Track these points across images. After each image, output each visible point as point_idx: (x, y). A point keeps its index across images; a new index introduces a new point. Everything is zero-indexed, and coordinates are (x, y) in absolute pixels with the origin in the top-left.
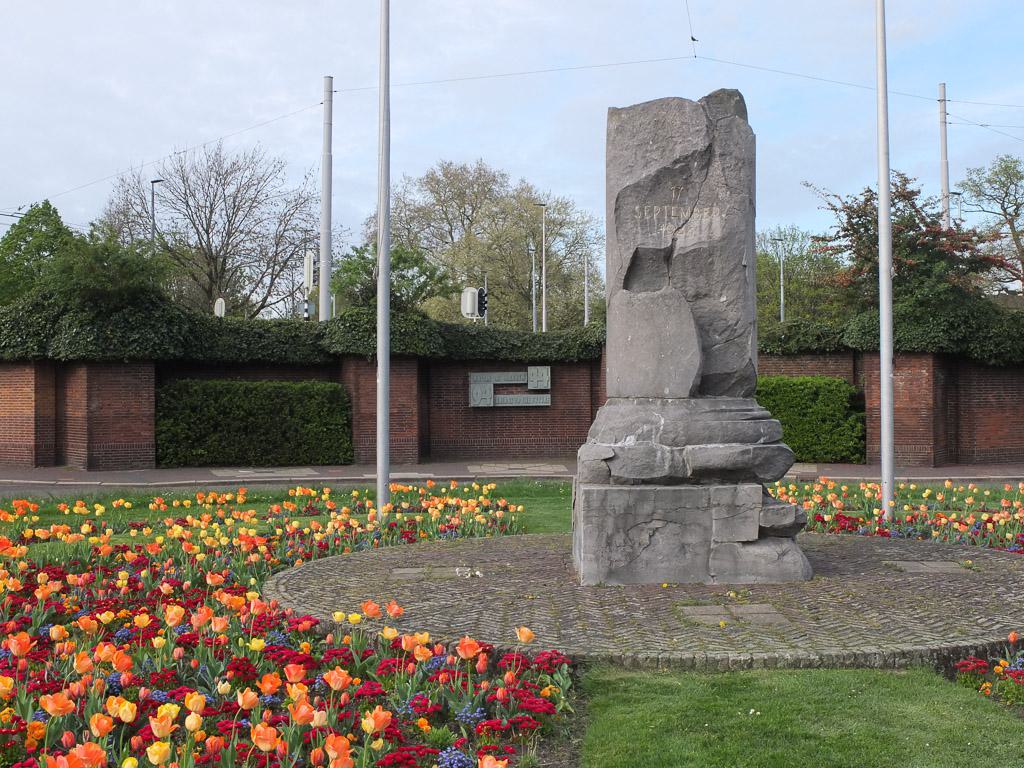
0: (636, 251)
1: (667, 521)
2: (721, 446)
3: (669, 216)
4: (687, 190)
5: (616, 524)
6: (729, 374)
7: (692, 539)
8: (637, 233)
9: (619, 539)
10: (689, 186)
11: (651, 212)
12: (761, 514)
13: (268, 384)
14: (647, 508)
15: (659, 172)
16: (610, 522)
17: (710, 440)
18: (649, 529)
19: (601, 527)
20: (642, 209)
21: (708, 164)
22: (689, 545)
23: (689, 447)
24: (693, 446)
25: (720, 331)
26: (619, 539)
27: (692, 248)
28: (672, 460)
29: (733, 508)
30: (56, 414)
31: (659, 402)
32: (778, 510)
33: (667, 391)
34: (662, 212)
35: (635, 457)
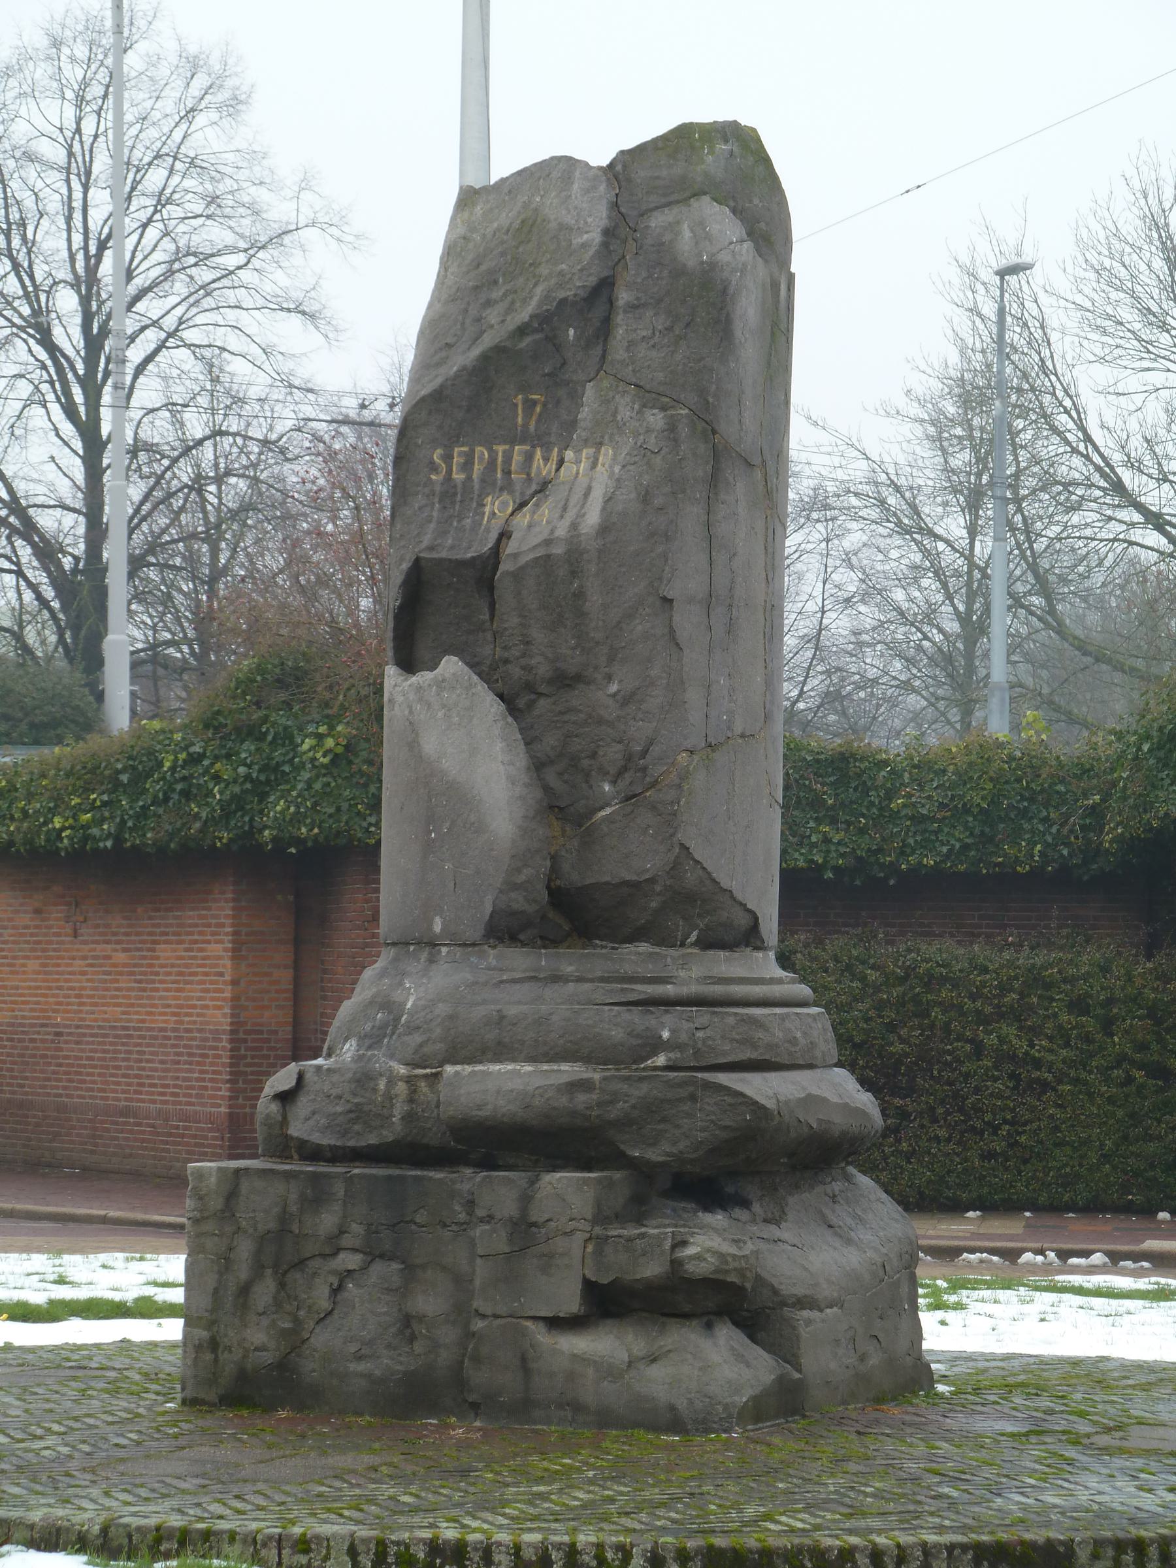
0: (417, 565)
1: (372, 1253)
2: (528, 1068)
3: (507, 473)
4: (558, 402)
5: (258, 1253)
6: (636, 885)
7: (429, 1302)
8: (429, 520)
9: (264, 1292)
10: (562, 392)
11: (467, 465)
12: (590, 1249)
13: (778, 1010)
14: (327, 1221)
15: (485, 358)
16: (245, 1249)
17: (501, 1051)
18: (334, 1272)
19: (225, 1262)
20: (448, 458)
21: (605, 329)
22: (421, 1318)
23: (449, 1069)
24: (458, 1068)
25: (613, 771)
26: (264, 1292)
27: (531, 556)
28: (411, 1100)
29: (524, 1230)
30: (296, 1023)
31: (424, 956)
32: (630, 1240)
33: (437, 927)
34: (492, 462)
35: (334, 1092)
